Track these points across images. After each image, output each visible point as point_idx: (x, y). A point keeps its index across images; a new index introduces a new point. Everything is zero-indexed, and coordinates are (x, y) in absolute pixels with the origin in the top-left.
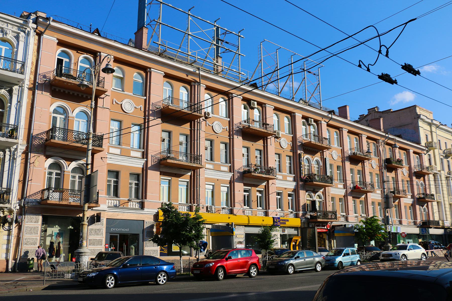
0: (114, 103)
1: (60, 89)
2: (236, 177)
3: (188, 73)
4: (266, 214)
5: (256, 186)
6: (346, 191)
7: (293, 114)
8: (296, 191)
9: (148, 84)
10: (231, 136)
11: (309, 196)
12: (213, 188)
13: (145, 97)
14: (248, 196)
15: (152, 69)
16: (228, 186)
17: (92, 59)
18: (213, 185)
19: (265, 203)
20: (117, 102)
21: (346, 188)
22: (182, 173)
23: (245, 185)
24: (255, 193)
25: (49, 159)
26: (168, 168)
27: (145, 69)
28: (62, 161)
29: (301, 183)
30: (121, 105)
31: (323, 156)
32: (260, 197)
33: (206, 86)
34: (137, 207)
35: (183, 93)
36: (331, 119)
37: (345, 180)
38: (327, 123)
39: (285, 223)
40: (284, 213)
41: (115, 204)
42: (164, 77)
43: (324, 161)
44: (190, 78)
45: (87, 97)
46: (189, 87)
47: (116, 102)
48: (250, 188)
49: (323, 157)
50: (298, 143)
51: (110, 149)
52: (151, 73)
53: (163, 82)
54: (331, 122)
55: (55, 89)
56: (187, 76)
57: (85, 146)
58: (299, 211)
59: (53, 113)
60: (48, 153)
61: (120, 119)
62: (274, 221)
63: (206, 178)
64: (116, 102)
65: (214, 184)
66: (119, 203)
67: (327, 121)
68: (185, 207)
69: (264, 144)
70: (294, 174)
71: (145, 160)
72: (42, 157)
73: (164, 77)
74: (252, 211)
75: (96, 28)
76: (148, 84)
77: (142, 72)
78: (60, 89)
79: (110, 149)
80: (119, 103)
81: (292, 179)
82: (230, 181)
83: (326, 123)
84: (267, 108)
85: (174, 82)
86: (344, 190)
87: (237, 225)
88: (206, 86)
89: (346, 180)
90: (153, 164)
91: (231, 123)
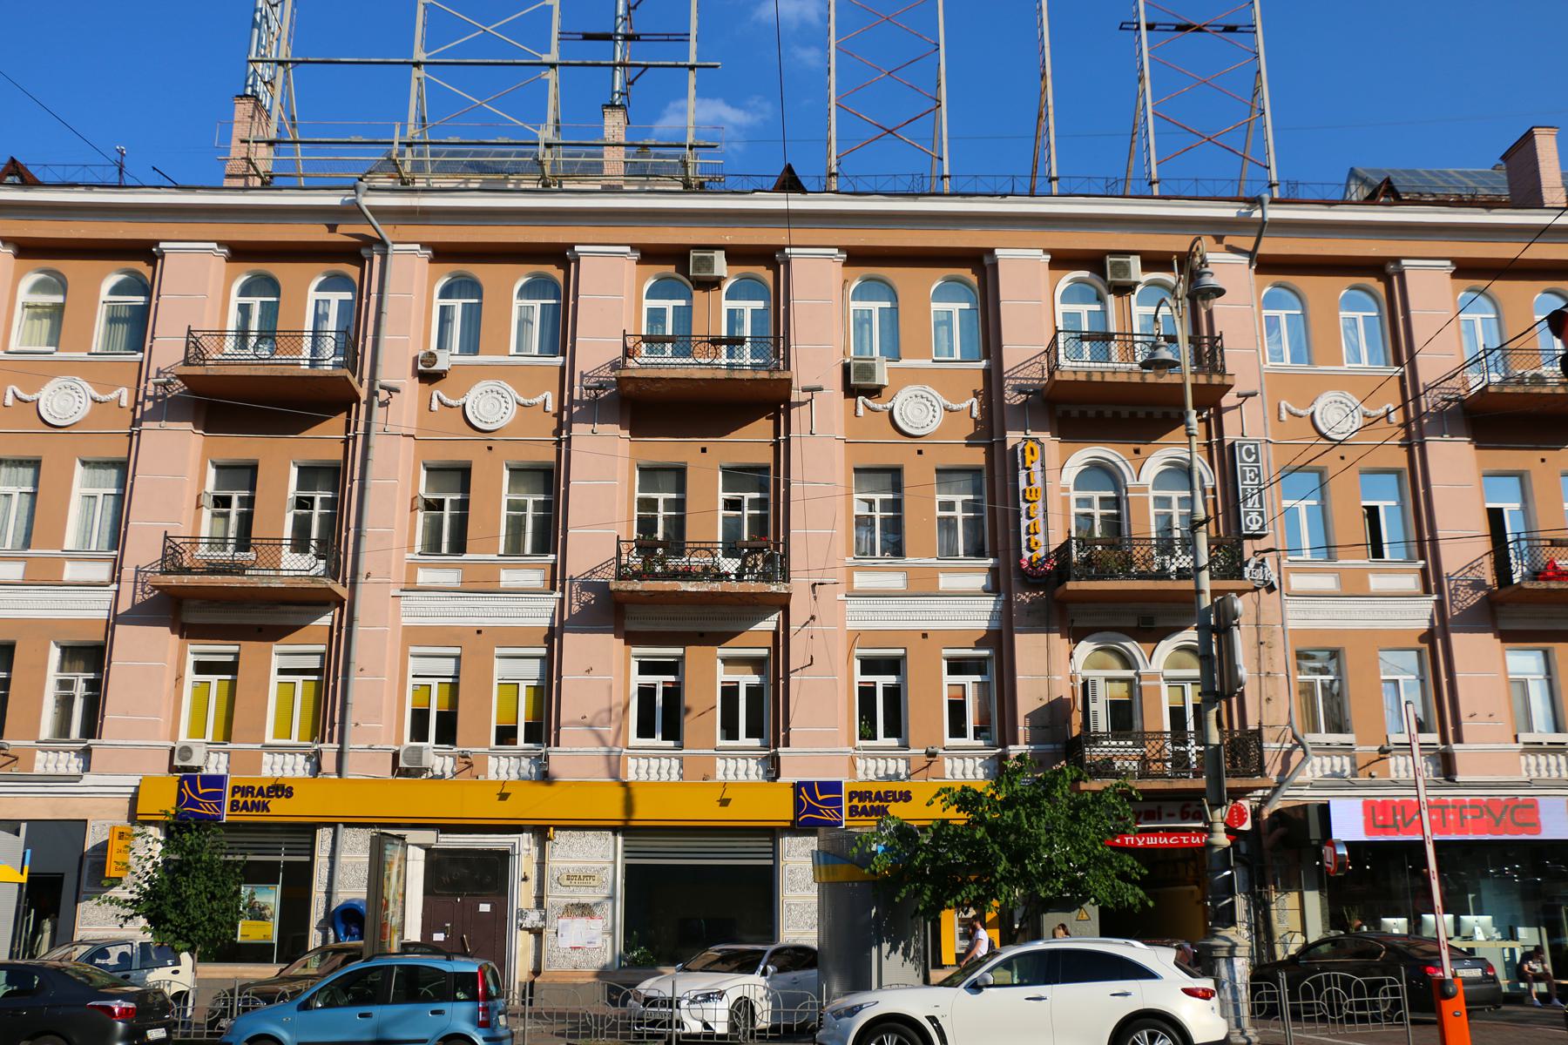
0: (1284, 416)
1: (1149, 409)
2: (125, 606)
3: (330, 216)
4: (773, 767)
5: (719, 639)
6: (1440, 604)
7: (987, 260)
8: (999, 640)
9: (1400, 318)
10: (1413, 442)
11: (1114, 661)
12: (458, 670)
13: (560, 359)
14: (893, 694)
15: (1404, 262)
16: (543, 652)
17: (974, 279)
18: (458, 658)
19: (762, 714)
20: (1293, 410)
21: (1440, 590)
22: (291, 621)
23: (632, 639)
24: (713, 672)
25: (1083, 644)
26: (211, 610)
27: (1379, 268)
28: (1128, 645)
29: (1025, 597)
30: (891, 412)
31: (1220, 433)
32: (750, 689)
33: (1454, 260)
34: (753, 777)
35: (1144, 312)
36: (1262, 228)
37: (1425, 543)
38: (1251, 255)
39: (265, 807)
40: (908, 760)
41: (891, 772)
42: (1454, 275)
43: (1225, 458)
44: (344, 233)
45: (1166, 416)
46: (1379, 287)
47: (1290, 412)
48: (679, 651)
49: (1221, 442)
50: (1008, 394)
51: (857, 577)
52: (1402, 275)
53: (1456, 293)
54: (1272, 246)
55: (1067, 414)
56: (332, 229)
57: (1188, 585)
58: (1186, 743)
59: (1077, 488)
60: (632, 626)
61: (28, 453)
62: (798, 804)
63: (407, 629)
64: (1290, 412)
65: (457, 651)
66: (908, 767)
67: (1247, 243)
68: (752, 763)
69: (777, 433)
70: (994, 556)
71: (1435, 597)
72: (1059, 642)
73: (1454, 275)
74: (681, 759)
75: (6, 160)
76: (1400, 318)
77: (966, 273)
78: (1149, 409)
79: (857, 577)
80: (1301, 412)
81: (980, 581)
82: (551, 629)
83: (1245, 260)
84: (1409, 275)
85: (1499, 287)
86: (1427, 605)
87: (347, 825)
88: (1454, 260)
89: (1434, 540)
90: (139, 599)
91: (1410, 389)
